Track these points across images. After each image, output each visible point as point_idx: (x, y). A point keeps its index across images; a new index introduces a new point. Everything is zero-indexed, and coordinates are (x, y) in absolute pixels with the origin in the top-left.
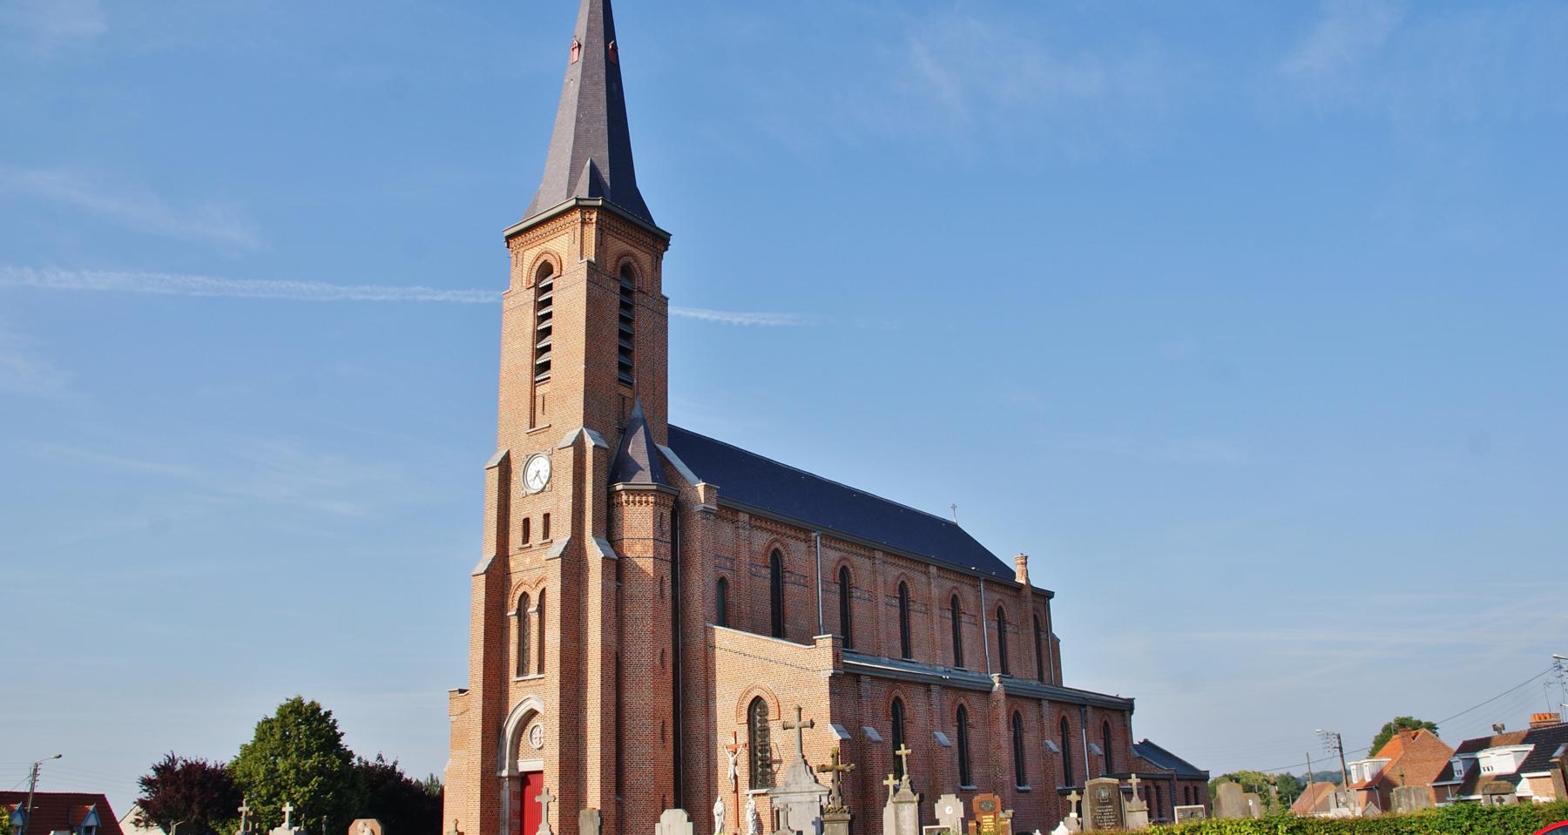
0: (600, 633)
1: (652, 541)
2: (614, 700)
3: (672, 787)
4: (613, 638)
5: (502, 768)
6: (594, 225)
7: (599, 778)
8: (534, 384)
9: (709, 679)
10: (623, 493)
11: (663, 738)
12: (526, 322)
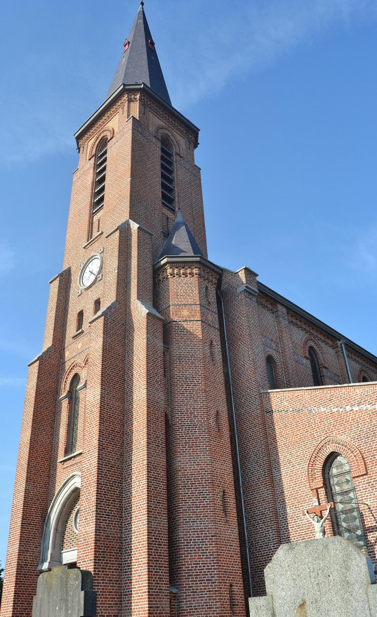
0: (145, 387)
1: (199, 306)
2: (164, 463)
3: (240, 572)
4: (161, 396)
5: (43, 562)
6: (138, 102)
7: (145, 560)
8: (92, 215)
9: (270, 447)
10: (168, 267)
11: (225, 511)
12: (89, 177)
